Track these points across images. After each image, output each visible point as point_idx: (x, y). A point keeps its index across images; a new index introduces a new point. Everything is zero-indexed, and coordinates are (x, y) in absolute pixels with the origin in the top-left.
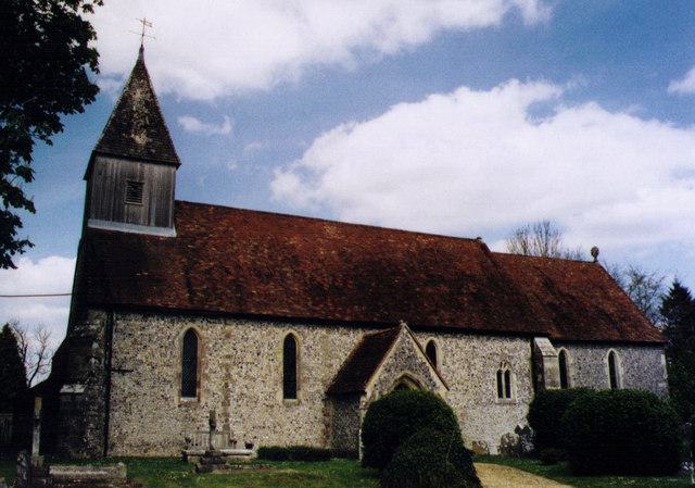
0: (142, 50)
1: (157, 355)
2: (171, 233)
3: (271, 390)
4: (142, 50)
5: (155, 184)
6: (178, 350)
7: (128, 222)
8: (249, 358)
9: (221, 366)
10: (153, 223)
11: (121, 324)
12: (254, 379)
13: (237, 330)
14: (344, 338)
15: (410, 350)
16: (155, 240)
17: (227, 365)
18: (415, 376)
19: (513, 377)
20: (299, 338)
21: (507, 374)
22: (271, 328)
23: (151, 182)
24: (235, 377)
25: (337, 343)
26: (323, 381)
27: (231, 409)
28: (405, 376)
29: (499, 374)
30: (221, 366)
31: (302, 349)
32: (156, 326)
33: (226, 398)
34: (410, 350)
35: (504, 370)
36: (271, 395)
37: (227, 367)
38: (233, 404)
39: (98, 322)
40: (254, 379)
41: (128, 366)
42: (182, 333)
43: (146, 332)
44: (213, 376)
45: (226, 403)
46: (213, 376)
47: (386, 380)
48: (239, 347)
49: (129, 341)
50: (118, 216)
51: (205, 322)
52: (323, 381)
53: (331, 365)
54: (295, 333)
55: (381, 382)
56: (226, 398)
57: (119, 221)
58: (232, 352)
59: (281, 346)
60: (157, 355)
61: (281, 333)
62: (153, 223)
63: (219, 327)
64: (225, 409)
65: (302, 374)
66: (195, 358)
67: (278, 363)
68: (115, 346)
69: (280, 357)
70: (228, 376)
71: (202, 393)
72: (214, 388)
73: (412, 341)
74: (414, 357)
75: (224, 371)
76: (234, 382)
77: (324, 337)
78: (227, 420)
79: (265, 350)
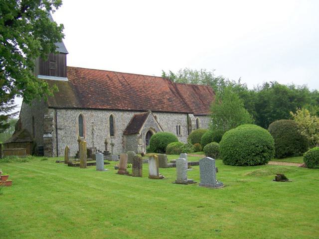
8: (99, 123)
11: (59, 113)
19: (181, 127)
21: (179, 127)
22: (105, 112)
29: (177, 126)
31: (115, 119)
35: (178, 125)
41: (62, 127)
53: (124, 125)
61: (109, 114)
65: (116, 128)
69: (109, 122)
70: (93, 129)
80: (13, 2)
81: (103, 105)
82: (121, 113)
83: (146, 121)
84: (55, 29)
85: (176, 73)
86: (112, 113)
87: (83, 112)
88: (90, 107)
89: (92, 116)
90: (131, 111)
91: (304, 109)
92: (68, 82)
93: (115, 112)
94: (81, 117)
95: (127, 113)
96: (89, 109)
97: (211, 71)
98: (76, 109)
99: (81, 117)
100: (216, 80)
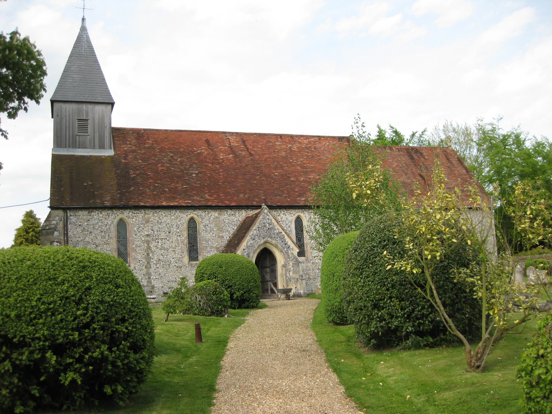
0: (83, 19)
1: (99, 237)
2: (110, 153)
3: (179, 256)
4: (83, 19)
5: (97, 121)
6: (113, 233)
7: (79, 148)
8: (163, 235)
9: (144, 242)
10: (67, 146)
11: (73, 219)
12: (167, 250)
13: (153, 216)
14: (232, 217)
15: (270, 224)
16: (100, 160)
17: (148, 241)
18: (274, 242)
20: (198, 219)
22: (178, 213)
23: (94, 120)
24: (154, 249)
25: (227, 221)
26: (217, 248)
27: (152, 270)
28: (266, 242)
30: (144, 242)
31: (200, 227)
32: (97, 216)
33: (148, 263)
34: (270, 224)
36: (180, 260)
37: (148, 242)
38: (153, 267)
39: (57, 218)
40: (167, 250)
42: (116, 221)
43: (90, 223)
44: (138, 249)
45: (148, 266)
46: (138, 249)
47: (252, 246)
48: (155, 228)
49: (79, 230)
50: (74, 145)
51: (131, 213)
52: (217, 248)
53: (223, 237)
54: (195, 216)
55: (248, 247)
56: (148, 263)
57: (73, 148)
58: (150, 232)
59: (185, 226)
60: (99, 237)
61: (185, 216)
62: (67, 146)
63: (141, 216)
64: (148, 271)
65: (201, 244)
66: (125, 238)
67: (183, 238)
68: (70, 233)
69: (185, 234)
70: (149, 248)
71: (132, 261)
72: (139, 257)
73: (271, 217)
74: (273, 228)
75: (146, 245)
76: (153, 253)
77: (217, 218)
78: (149, 278)
79: (174, 229)
80: (4, 50)
81: (174, 198)
82: (214, 214)
83: (254, 228)
84: (480, 141)
85: (406, 135)
86: (300, 214)
87: (126, 215)
88: (142, 204)
89: (147, 222)
90: (239, 207)
91: (27, 349)
92: (112, 157)
93: (200, 212)
94: (122, 224)
95: (230, 212)
96: (137, 208)
97: (495, 122)
98: (111, 208)
99: (122, 224)
100: (505, 138)
